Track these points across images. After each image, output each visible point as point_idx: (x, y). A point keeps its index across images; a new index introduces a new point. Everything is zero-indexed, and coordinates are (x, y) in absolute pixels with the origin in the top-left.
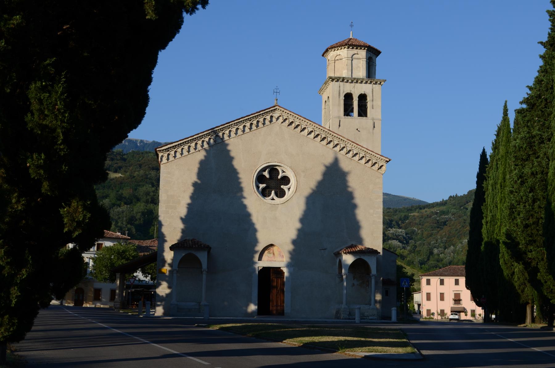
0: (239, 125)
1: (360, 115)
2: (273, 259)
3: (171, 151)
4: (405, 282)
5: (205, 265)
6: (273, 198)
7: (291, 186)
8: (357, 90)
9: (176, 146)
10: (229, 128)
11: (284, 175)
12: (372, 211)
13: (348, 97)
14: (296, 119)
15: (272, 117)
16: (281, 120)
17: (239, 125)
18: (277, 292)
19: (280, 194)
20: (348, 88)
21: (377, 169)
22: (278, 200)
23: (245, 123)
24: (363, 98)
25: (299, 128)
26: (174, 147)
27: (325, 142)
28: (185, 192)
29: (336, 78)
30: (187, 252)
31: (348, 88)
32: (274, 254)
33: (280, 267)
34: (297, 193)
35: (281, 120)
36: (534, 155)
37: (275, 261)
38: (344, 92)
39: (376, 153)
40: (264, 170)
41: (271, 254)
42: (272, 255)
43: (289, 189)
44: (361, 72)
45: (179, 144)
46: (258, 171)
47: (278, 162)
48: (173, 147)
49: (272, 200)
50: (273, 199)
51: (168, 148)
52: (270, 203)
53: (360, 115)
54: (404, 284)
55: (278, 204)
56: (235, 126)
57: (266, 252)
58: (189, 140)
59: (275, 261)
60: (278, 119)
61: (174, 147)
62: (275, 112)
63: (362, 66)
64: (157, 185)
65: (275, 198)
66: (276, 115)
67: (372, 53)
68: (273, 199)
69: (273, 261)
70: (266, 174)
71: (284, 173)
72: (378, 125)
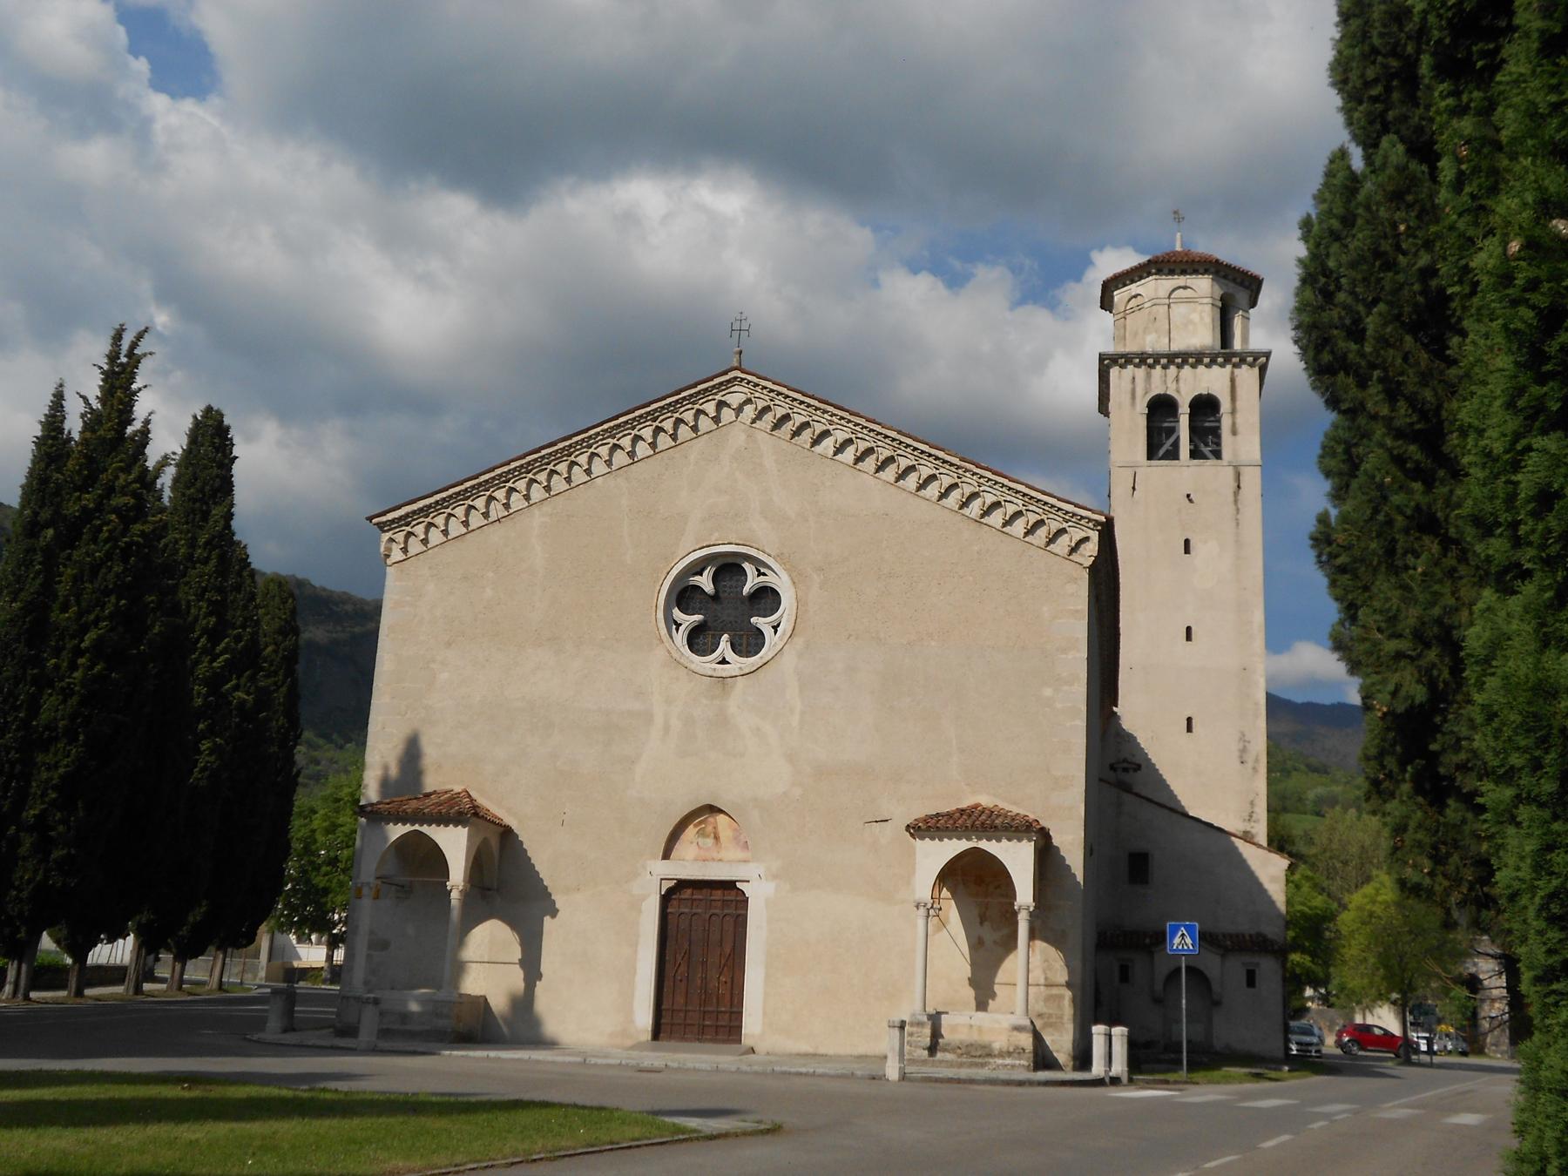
0: (621, 435)
1: (1195, 454)
2: (715, 855)
3: (418, 524)
4: (1183, 935)
5: (1025, 894)
6: (724, 658)
7: (782, 616)
8: (1187, 385)
9: (430, 506)
10: (590, 446)
11: (761, 585)
12: (1048, 692)
13: (1161, 408)
14: (779, 400)
15: (721, 405)
16: (749, 411)
17: (621, 435)
18: (723, 962)
19: (749, 643)
20: (1161, 381)
21: (1067, 550)
22: (738, 663)
23: (638, 427)
24: (1205, 406)
25: (807, 435)
26: (425, 511)
27: (890, 473)
28: (450, 645)
29: (1122, 356)
30: (408, 828)
31: (1161, 381)
32: (716, 838)
33: (734, 878)
34: (795, 639)
35: (749, 411)
36: (1319, 269)
37: (720, 860)
38: (1146, 393)
39: (1059, 499)
40: (697, 568)
41: (708, 836)
42: (710, 841)
43: (775, 628)
44: (1199, 331)
45: (437, 502)
46: (675, 572)
47: (738, 542)
48: (421, 510)
49: (719, 663)
50: (724, 662)
51: (407, 515)
52: (710, 673)
53: (1195, 454)
54: (1179, 944)
55: (734, 674)
56: (609, 440)
57: (691, 831)
58: (466, 489)
59: (720, 860)
60: (739, 410)
61: (425, 511)
62: (732, 390)
63: (1202, 318)
64: (1287, 773)
65: (730, 655)
66: (735, 399)
67: (1234, 280)
68: (724, 662)
69: (713, 860)
70: (705, 582)
71: (762, 578)
72: (1252, 480)
